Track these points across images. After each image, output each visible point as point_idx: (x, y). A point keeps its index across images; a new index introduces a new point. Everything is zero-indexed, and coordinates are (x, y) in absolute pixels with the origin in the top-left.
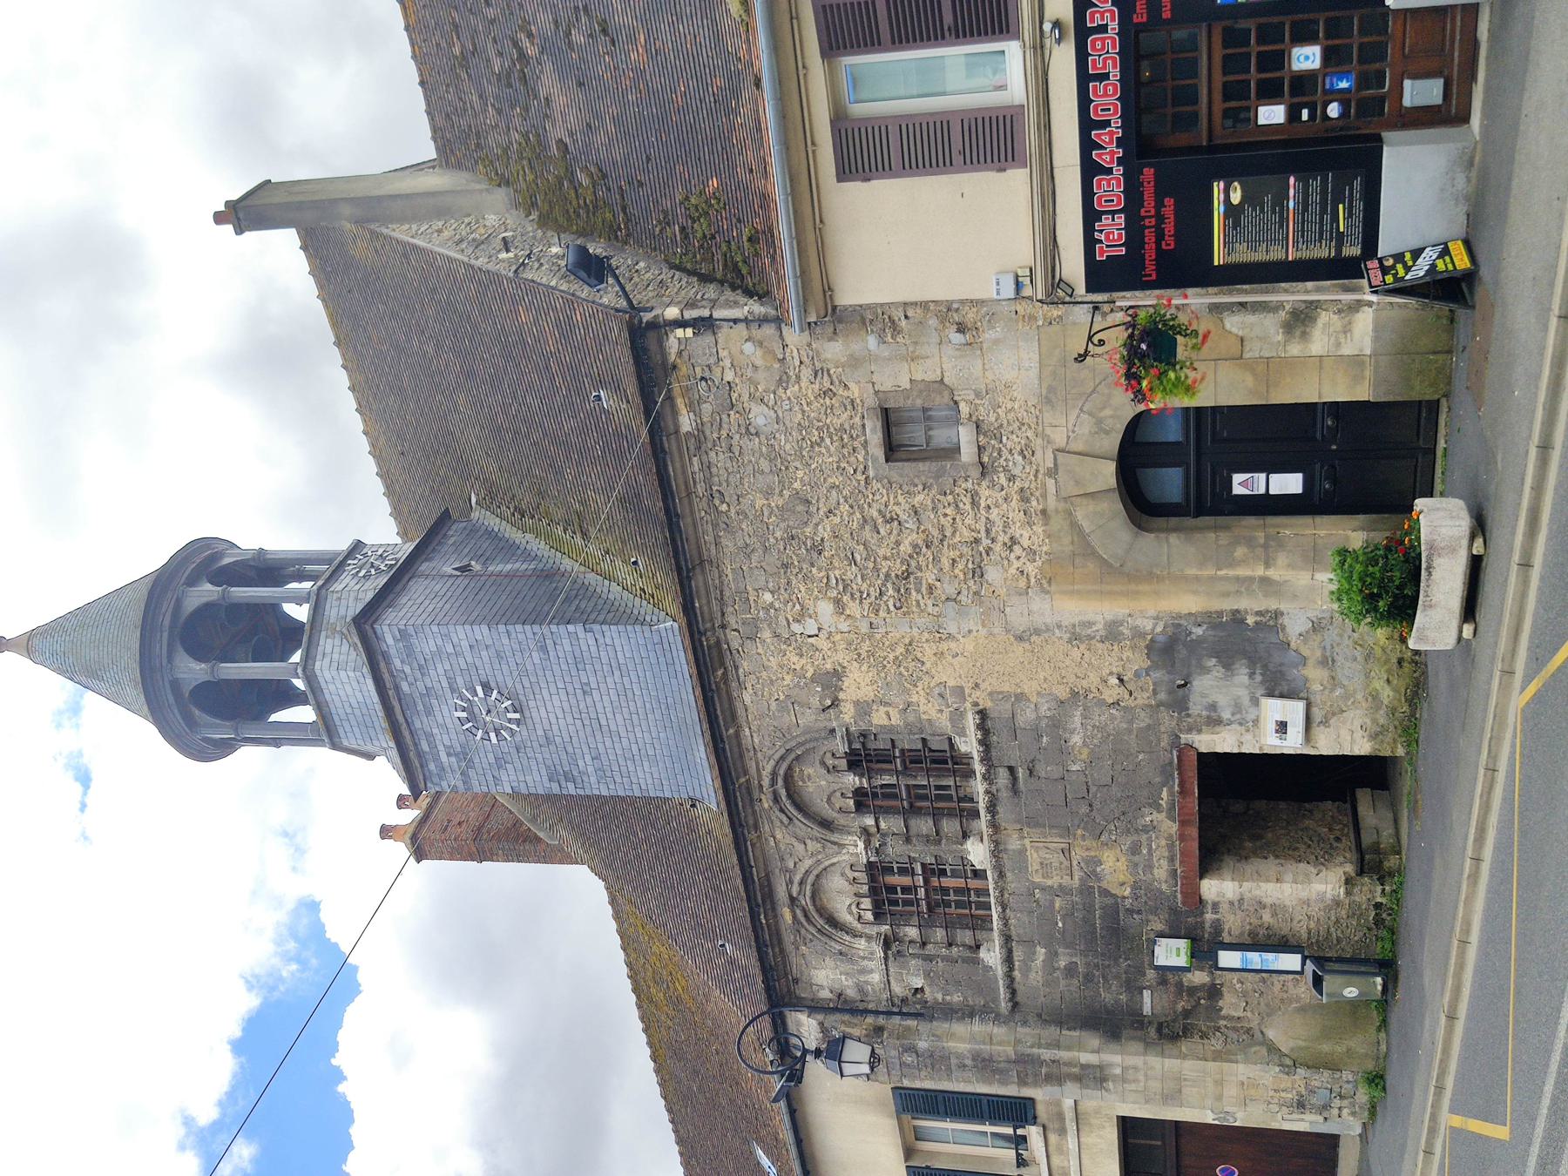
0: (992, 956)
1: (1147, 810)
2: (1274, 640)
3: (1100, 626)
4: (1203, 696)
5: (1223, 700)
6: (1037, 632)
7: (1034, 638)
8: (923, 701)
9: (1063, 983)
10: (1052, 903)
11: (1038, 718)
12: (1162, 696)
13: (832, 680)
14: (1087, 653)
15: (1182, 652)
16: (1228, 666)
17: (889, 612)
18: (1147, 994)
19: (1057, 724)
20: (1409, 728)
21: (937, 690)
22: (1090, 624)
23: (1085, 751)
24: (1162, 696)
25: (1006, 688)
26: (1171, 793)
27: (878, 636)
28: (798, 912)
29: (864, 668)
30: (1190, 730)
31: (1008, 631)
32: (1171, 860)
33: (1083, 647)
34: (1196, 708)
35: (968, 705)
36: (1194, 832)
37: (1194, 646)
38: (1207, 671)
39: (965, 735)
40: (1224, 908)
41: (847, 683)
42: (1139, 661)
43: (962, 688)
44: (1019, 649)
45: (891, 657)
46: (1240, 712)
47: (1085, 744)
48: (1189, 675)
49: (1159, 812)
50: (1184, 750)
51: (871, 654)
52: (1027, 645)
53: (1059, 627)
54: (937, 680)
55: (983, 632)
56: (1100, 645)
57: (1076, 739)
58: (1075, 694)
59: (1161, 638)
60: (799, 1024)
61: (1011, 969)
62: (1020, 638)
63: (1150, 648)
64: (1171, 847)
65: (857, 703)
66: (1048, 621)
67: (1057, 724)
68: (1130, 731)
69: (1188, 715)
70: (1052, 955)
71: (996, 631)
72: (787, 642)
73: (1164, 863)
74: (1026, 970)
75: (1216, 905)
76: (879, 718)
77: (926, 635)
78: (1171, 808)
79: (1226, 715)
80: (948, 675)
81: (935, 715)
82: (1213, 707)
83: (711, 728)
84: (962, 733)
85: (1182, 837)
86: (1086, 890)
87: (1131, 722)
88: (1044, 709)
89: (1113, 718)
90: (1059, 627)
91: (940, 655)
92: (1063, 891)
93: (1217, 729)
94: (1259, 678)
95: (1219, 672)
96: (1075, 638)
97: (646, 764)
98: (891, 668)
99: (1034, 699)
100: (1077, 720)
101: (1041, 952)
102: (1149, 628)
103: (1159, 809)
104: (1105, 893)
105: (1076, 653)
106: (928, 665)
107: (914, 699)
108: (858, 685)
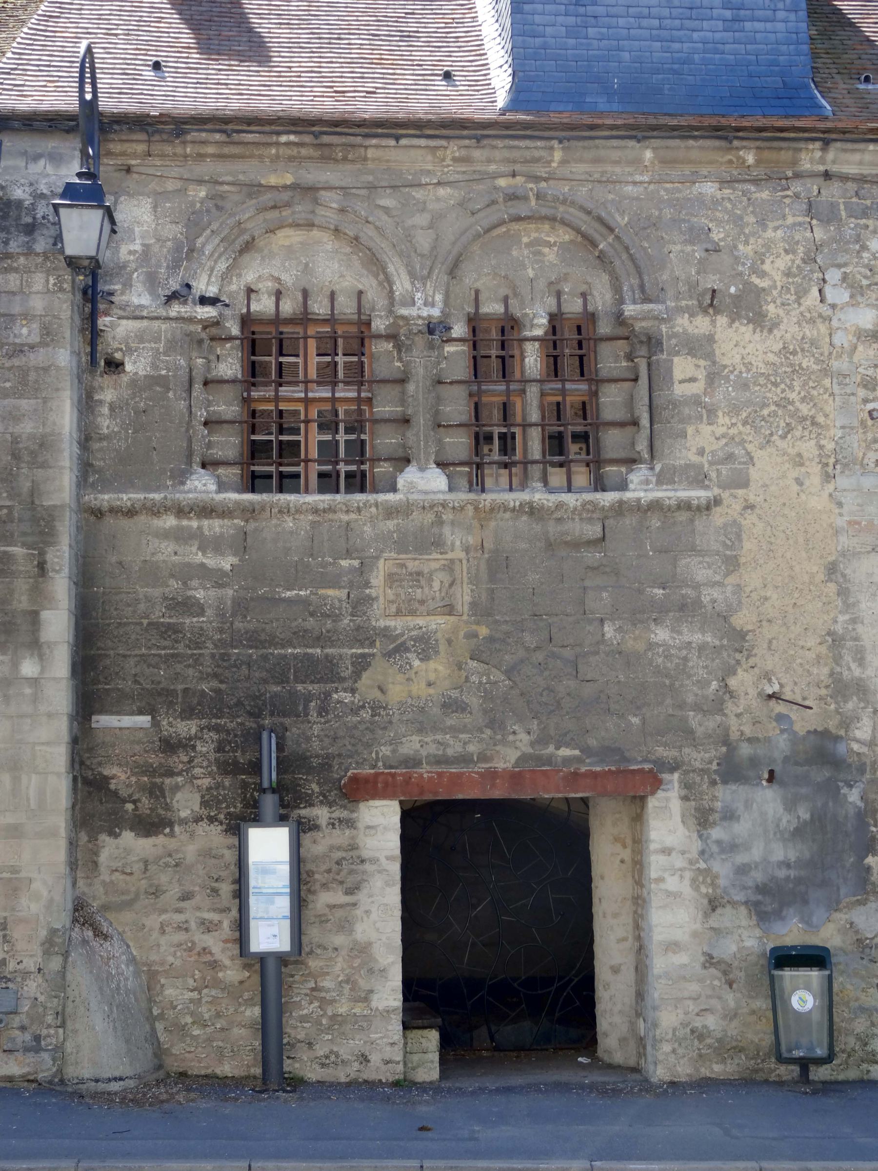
0: (202, 485)
1: (534, 725)
2: (843, 891)
3: (857, 672)
4: (748, 805)
5: (742, 828)
6: (843, 593)
7: (832, 587)
8: (720, 431)
9: (156, 593)
10: (335, 584)
11: (697, 587)
12: (745, 750)
13: (748, 307)
14: (811, 655)
15: (821, 774)
16: (798, 833)
17: (866, 401)
18: (144, 720)
19: (686, 609)
20: (772, 978)
21: (738, 451)
22: (861, 661)
23: (641, 646)
24: (745, 750)
25: (747, 545)
26: (567, 761)
27: (827, 382)
28: (285, 196)
29: (771, 358)
30: (687, 785)
31: (843, 554)
32: (439, 761)
33: (823, 650)
34: (725, 795)
35: (716, 491)
36: (497, 793)
37: (831, 789)
38: (790, 805)
39: (659, 482)
40: (340, 837)
41: (745, 331)
42: (804, 723)
43: (745, 484)
44: (816, 569)
45: (793, 396)
46: (723, 851)
47: (651, 646)
48: (782, 784)
49: (532, 744)
50: (635, 788)
51: (797, 370)
52: (821, 577)
53: (854, 621)
54: (757, 454)
55: (841, 522)
56: (826, 671)
57: (661, 634)
58: (742, 635)
59: (841, 748)
60: (56, 159)
61: (181, 511)
62: (832, 570)
63: (825, 734)
64: (465, 759)
65: (710, 339)
66: (863, 606)
67: (686, 609)
68: (682, 706)
69: (713, 783)
70: (218, 579)
71: (843, 539)
72: (809, 259)
73: (432, 749)
74: (180, 536)
75: (350, 823)
76: (683, 367)
77: (830, 446)
78: (539, 760)
79: (716, 833)
80: (766, 466)
81: (698, 442)
82: (730, 816)
83: (428, 124)
84: (662, 480)
85: (492, 775)
86: (364, 635)
87: (697, 708)
88: (708, 595)
89: (703, 684)
90: (854, 621)
91: (799, 461)
92: (360, 603)
93: (692, 822)
94: (782, 873)
95: (787, 821)
96: (835, 641)
97: (571, 20)
98: (774, 394)
99: (731, 580)
100: (697, 638)
101: (227, 563)
102: (858, 734)
103: (542, 740)
104: (362, 664)
105: (812, 641)
106: (779, 443)
107: (723, 419)
108: (739, 345)
